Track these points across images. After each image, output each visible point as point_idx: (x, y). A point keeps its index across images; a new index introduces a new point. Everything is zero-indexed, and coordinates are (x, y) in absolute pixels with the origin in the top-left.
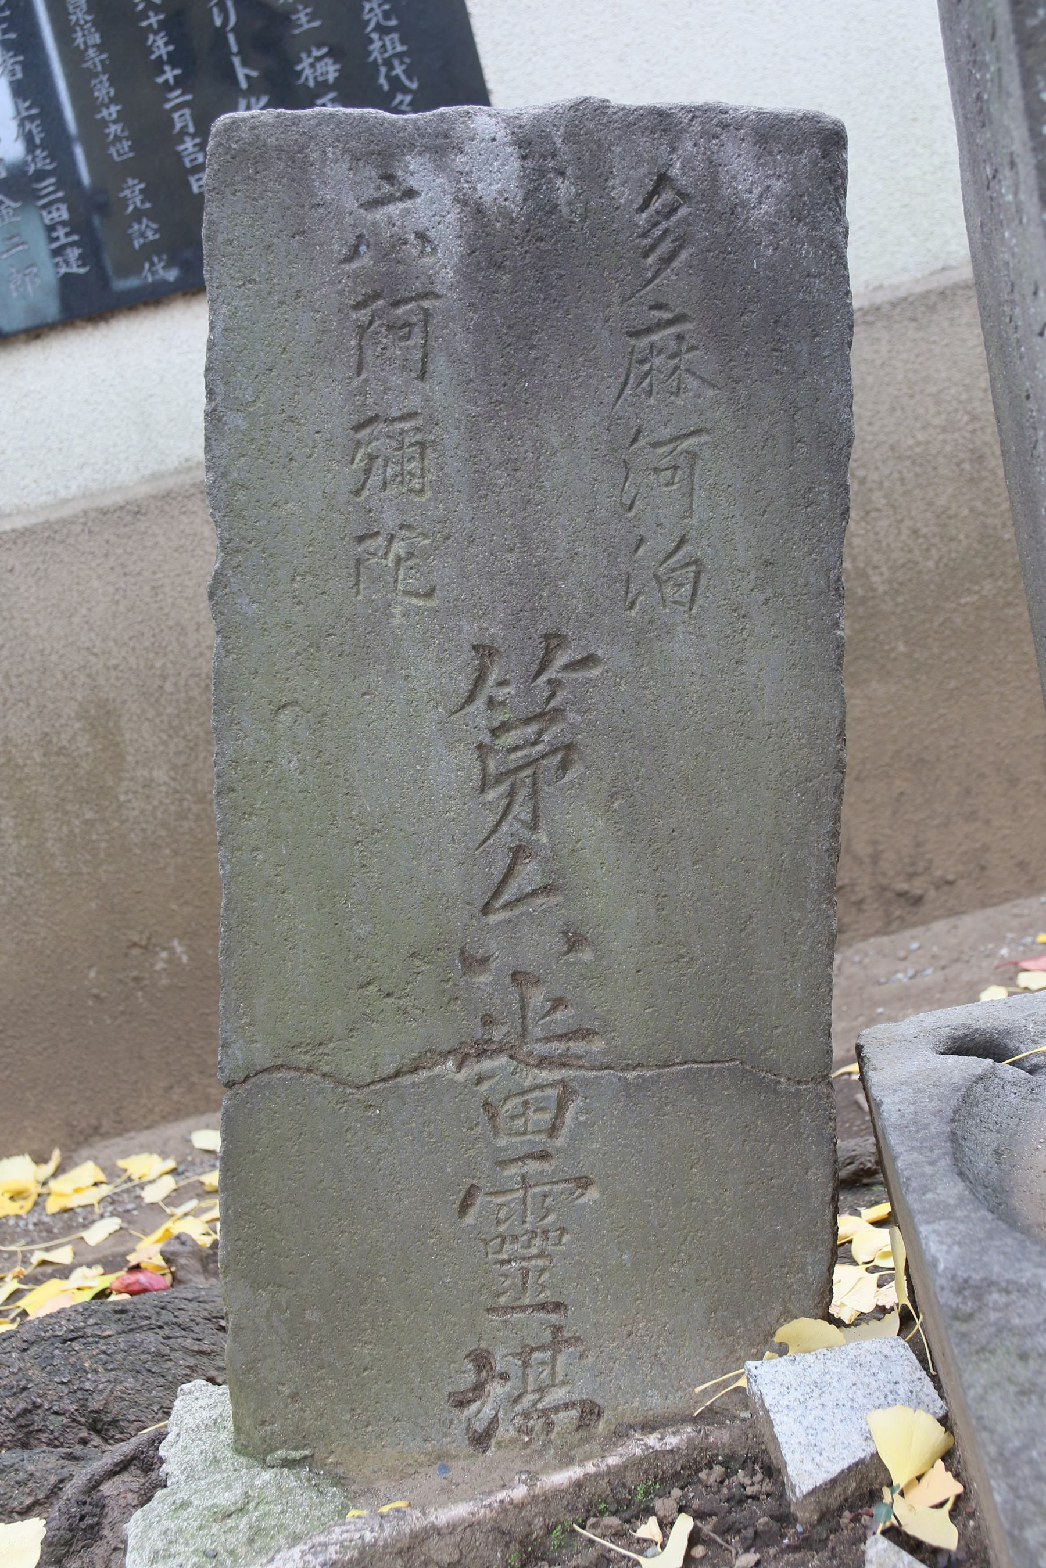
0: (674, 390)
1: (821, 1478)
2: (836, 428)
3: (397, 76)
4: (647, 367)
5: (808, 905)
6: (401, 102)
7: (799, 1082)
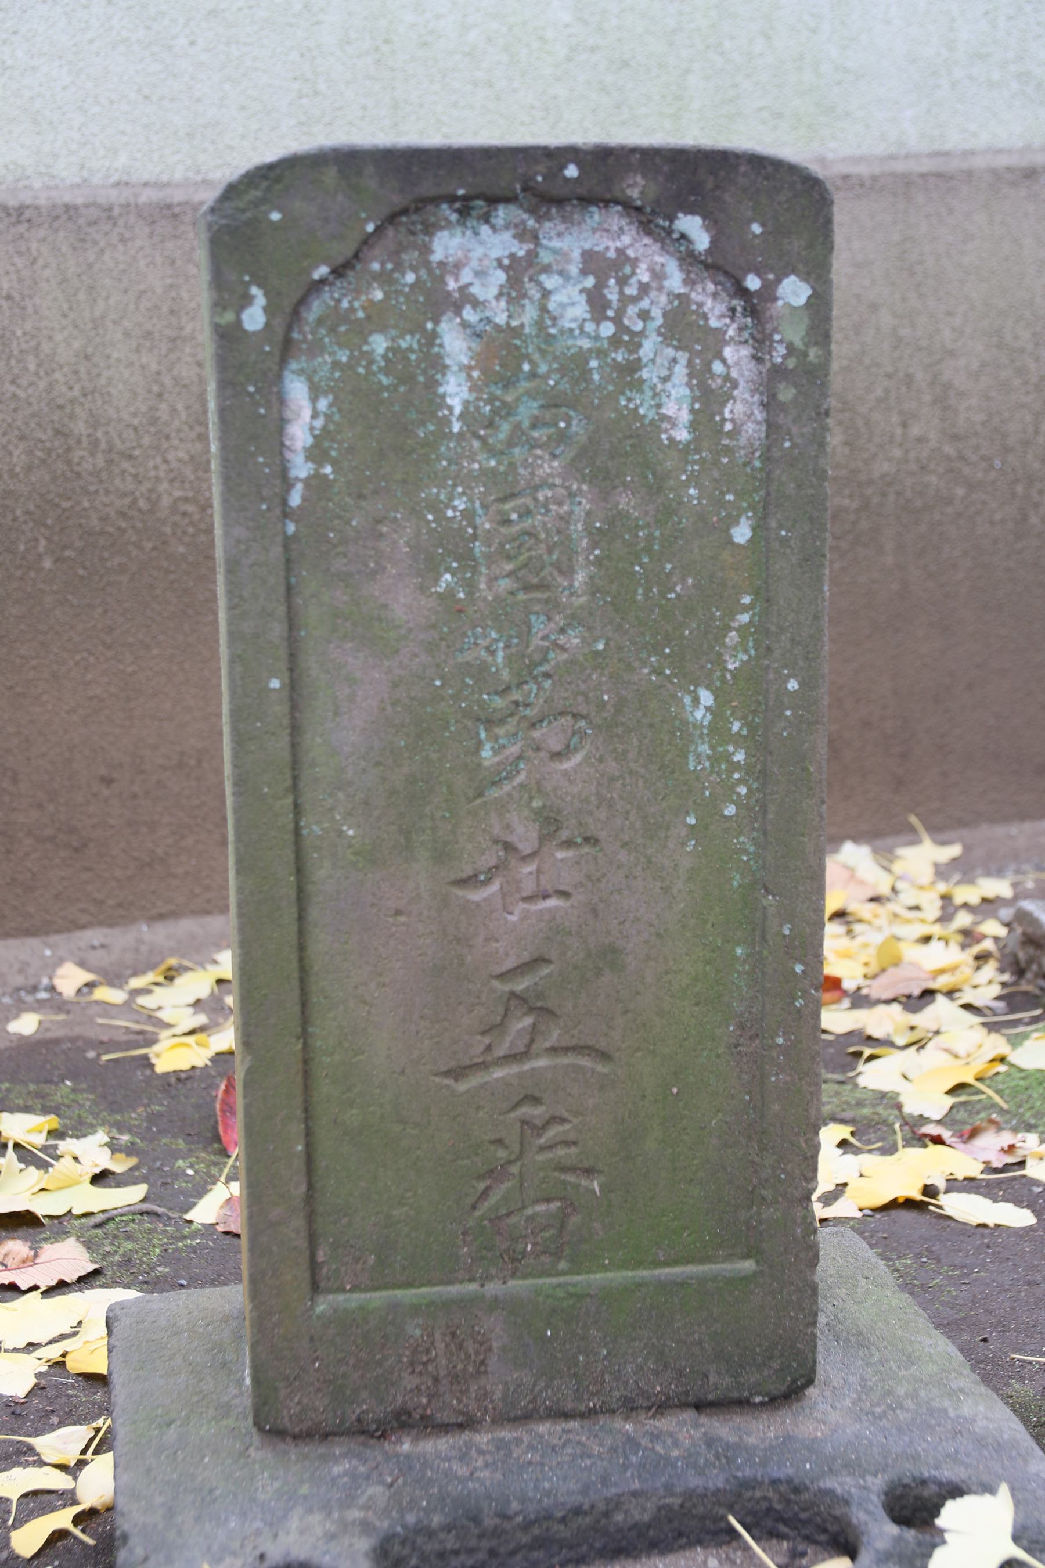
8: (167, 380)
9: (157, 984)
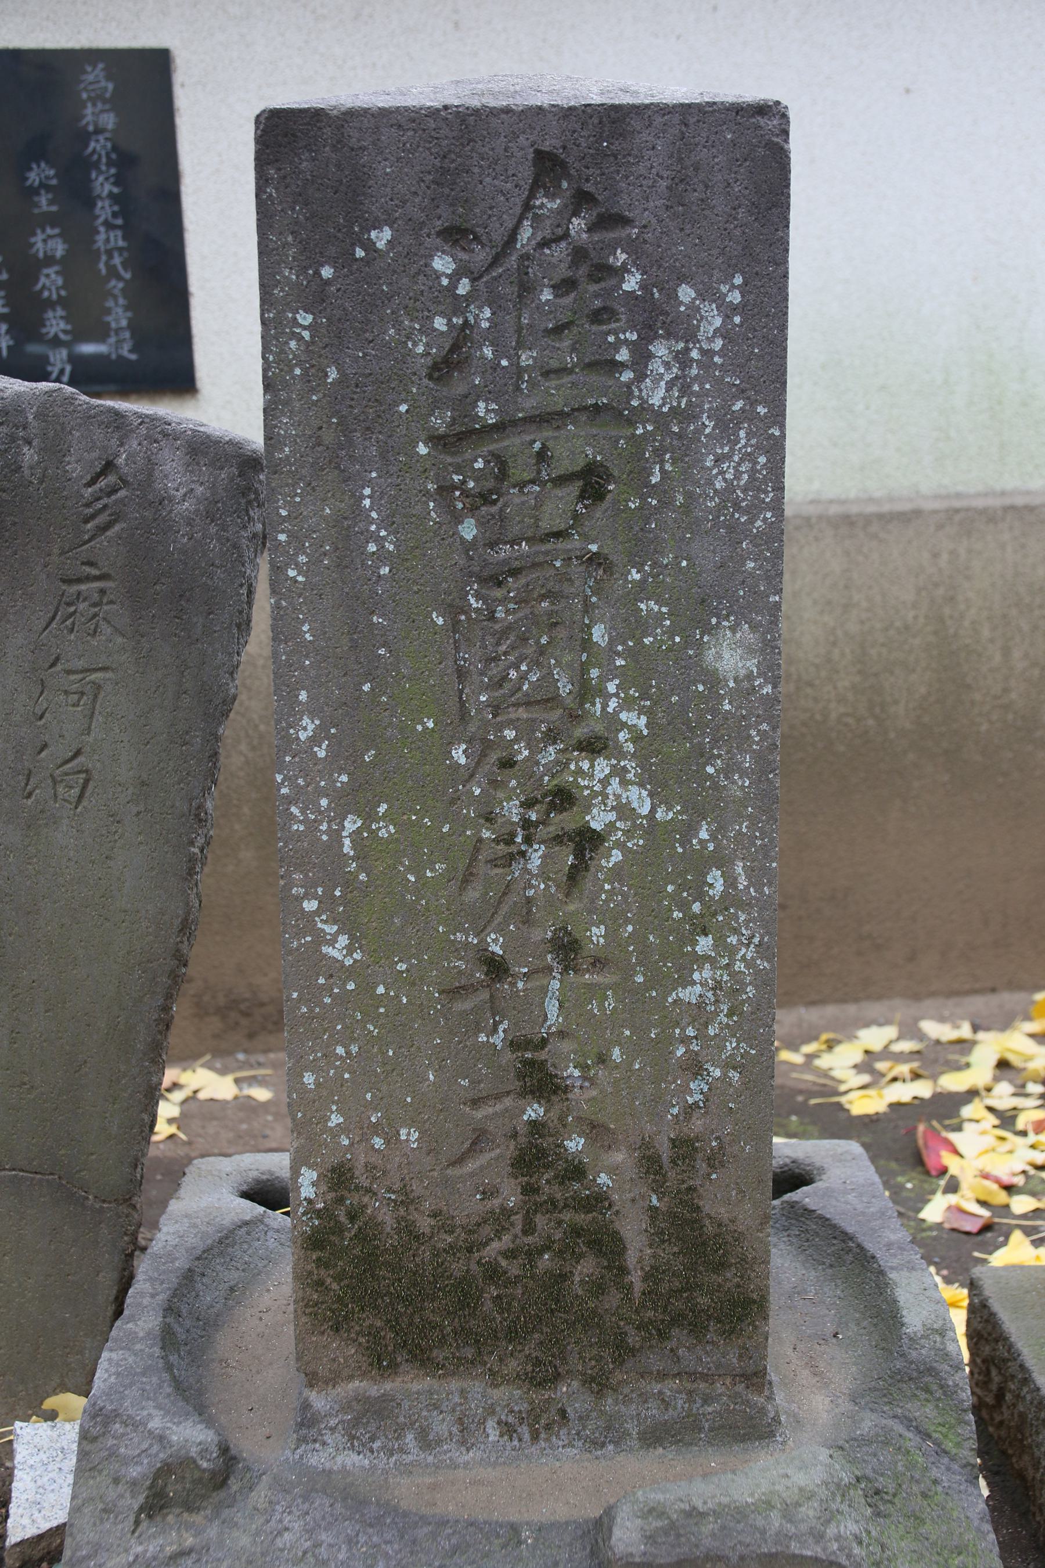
0: (91, 632)
1: (31, 1532)
2: (215, 688)
3: (115, 266)
4: (72, 609)
5: (134, 1061)
6: (115, 287)
7: (104, 1201)
8: (839, 633)
9: (821, 1051)
